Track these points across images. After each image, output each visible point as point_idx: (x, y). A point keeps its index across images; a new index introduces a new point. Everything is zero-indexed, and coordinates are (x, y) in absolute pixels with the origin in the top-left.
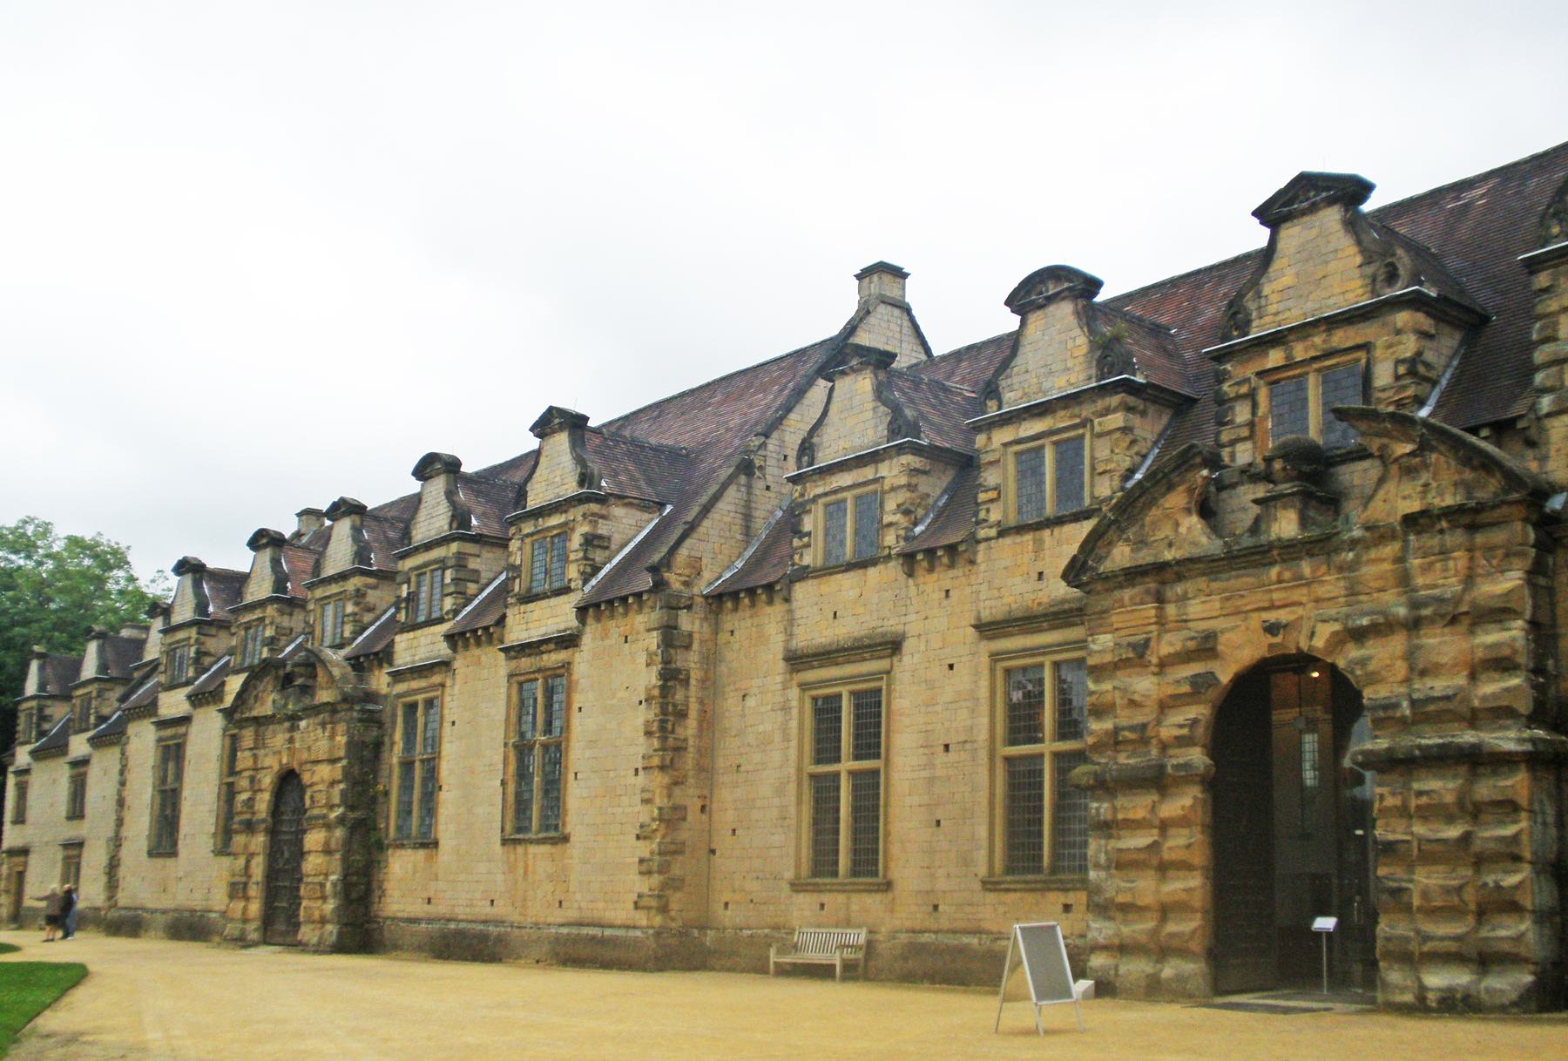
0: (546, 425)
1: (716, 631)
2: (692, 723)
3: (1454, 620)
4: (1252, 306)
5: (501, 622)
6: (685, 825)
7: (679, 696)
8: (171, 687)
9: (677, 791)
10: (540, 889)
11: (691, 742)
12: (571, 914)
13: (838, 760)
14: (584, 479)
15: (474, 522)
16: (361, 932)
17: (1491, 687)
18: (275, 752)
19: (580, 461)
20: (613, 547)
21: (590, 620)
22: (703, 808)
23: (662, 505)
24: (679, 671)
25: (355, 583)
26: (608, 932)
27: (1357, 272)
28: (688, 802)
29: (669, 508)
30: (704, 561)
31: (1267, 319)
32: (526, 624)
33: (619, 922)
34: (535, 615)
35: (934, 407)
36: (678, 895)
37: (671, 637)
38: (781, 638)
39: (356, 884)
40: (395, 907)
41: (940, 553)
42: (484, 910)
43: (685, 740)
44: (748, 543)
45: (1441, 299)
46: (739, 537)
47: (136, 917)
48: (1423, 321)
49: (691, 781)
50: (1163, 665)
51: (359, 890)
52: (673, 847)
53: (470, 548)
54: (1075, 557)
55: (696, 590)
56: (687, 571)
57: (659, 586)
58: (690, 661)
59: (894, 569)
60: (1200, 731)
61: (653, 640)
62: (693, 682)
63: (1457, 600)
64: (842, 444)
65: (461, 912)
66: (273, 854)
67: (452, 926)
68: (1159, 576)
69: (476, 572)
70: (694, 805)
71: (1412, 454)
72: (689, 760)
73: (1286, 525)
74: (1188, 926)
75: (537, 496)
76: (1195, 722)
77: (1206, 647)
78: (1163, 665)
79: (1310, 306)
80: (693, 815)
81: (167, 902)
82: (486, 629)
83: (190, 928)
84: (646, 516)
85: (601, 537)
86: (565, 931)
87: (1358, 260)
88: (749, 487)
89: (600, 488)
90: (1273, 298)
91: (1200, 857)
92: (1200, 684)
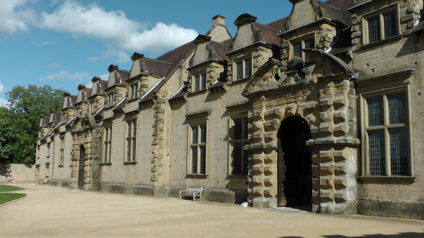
4: (289, 23)
6: (163, 159)
8: (62, 125)
9: (161, 150)
10: (140, 174)
11: (164, 138)
12: (138, 182)
13: (241, 138)
14: (142, 71)
15: (121, 82)
16: (98, 187)
19: (141, 66)
20: (149, 88)
21: (142, 106)
23: (162, 77)
24: (161, 119)
26: (145, 187)
27: (312, 14)
28: (163, 153)
29: (164, 77)
30: (168, 91)
31: (292, 27)
32: (128, 109)
33: (147, 184)
34: (131, 105)
35: (223, 51)
36: (161, 177)
38: (185, 110)
39: (95, 174)
40: (104, 180)
41: (218, 88)
42: (121, 180)
43: (163, 137)
44: (180, 86)
45: (333, 21)
46: (178, 85)
47: (56, 181)
49: (165, 148)
51: (97, 176)
52: (159, 165)
54: (245, 89)
55: (166, 98)
56: (163, 94)
62: (165, 122)
64: (199, 60)
65: (116, 181)
66: (80, 165)
67: (114, 184)
69: (121, 94)
71: (321, 61)
73: (292, 81)
79: (301, 23)
81: (62, 178)
83: (65, 184)
84: (158, 79)
85: (146, 85)
86: (137, 186)
87: (313, 11)
88: (181, 72)
89: (146, 73)
90: (294, 21)
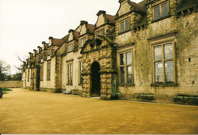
0: (69, 32)
1: (62, 59)
2: (59, 68)
3: (105, 58)
5: (47, 58)
7: (58, 66)
16: (38, 89)
17: (108, 66)
18: (92, 57)
22: (61, 77)
25: (39, 54)
37: (56, 59)
48: (108, 26)
50: (87, 62)
53: (45, 51)
57: (56, 54)
58: (59, 62)
59: (72, 52)
60: (89, 69)
61: (55, 60)
63: (105, 56)
68: (87, 53)
70: (60, 77)
72: (59, 72)
74: (88, 90)
75: (70, 40)
76: (89, 68)
77: (90, 61)
78: (87, 62)
80: (60, 78)
82: (76, 50)
91: (89, 82)
92: (89, 64)
